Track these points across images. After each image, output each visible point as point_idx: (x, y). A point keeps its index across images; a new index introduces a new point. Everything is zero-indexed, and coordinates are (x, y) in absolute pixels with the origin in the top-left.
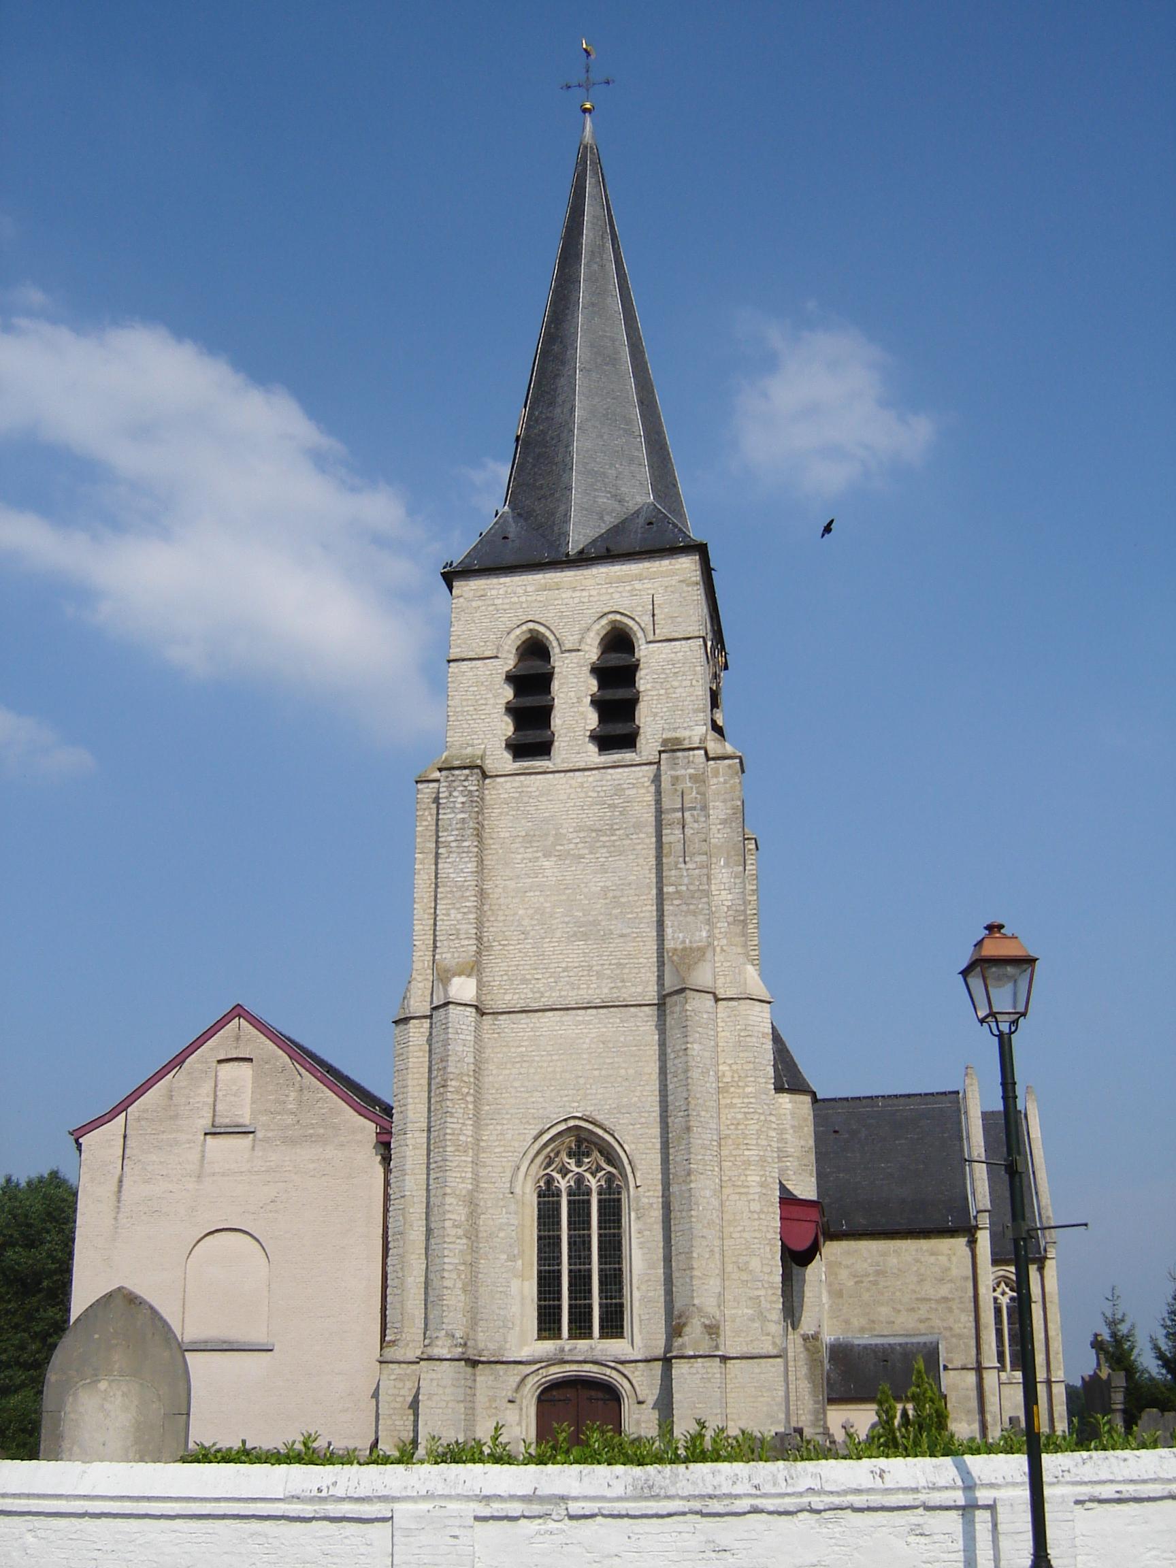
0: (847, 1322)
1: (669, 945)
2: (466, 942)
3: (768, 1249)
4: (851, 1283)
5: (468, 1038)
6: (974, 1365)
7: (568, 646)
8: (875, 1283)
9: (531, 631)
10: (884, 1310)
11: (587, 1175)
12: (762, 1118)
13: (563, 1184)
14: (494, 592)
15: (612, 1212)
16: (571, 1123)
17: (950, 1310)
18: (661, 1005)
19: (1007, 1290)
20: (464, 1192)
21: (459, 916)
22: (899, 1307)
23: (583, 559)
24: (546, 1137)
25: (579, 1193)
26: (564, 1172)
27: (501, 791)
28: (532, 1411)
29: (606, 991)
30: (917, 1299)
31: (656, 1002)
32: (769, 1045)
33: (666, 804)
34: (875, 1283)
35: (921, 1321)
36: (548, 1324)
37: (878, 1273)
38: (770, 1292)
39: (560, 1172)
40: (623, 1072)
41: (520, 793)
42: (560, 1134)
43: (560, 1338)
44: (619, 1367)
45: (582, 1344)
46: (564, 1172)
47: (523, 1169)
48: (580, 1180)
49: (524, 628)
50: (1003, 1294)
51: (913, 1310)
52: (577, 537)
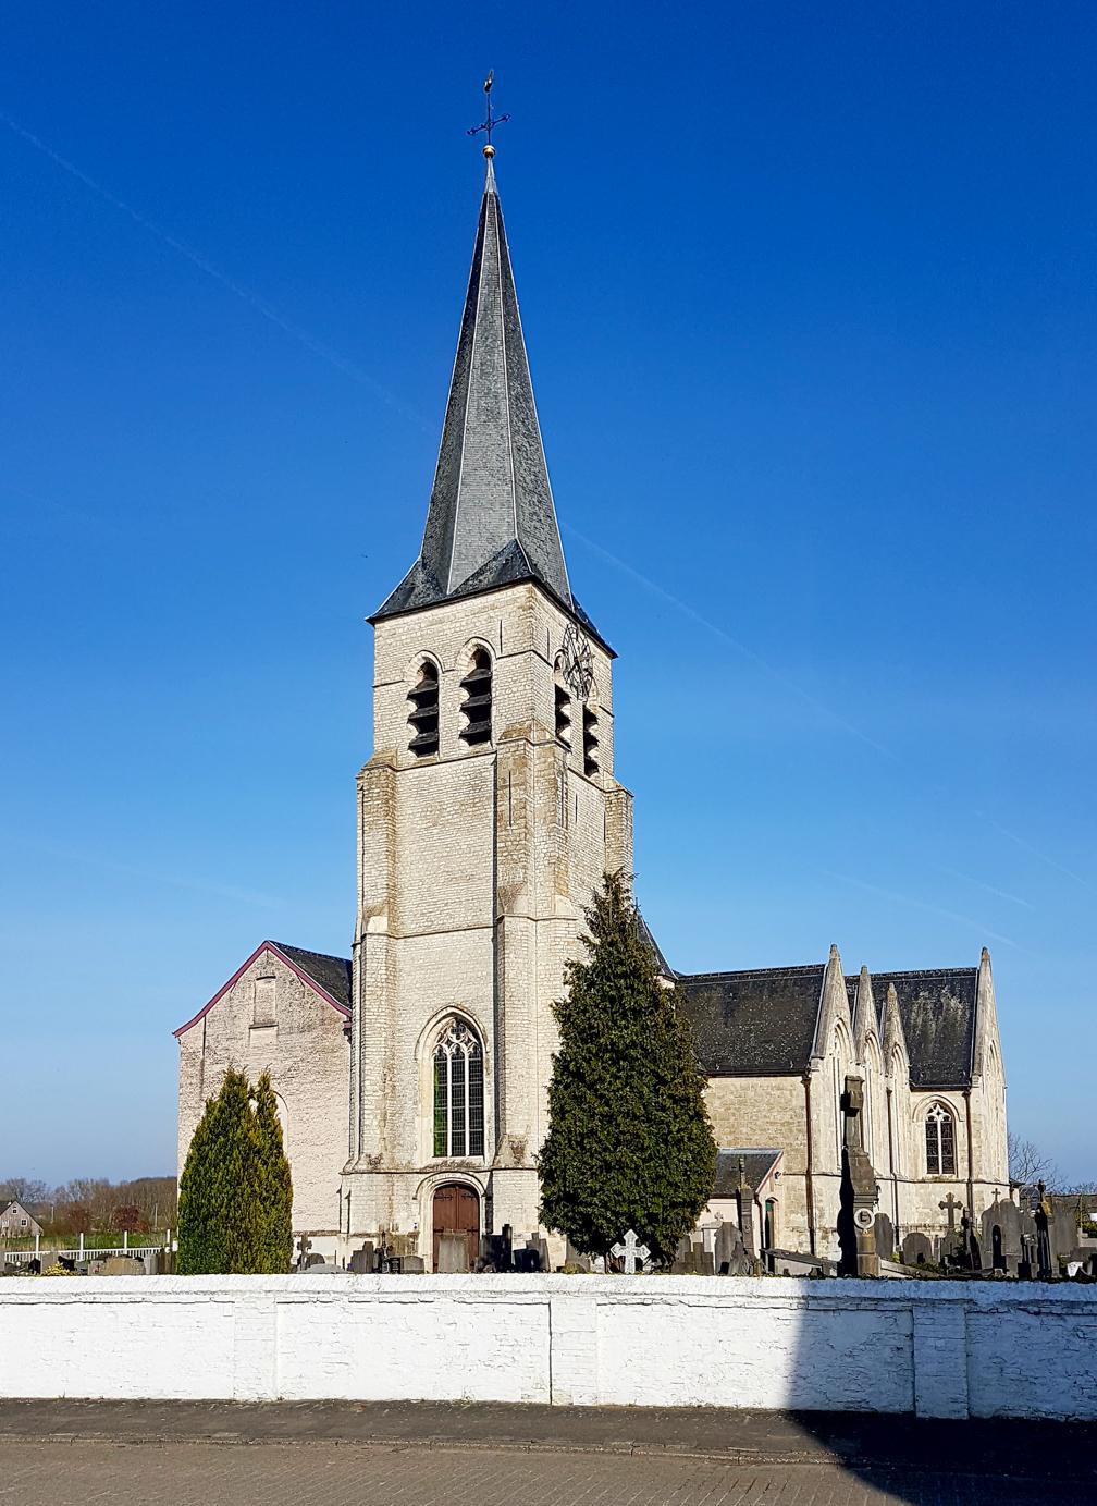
1: (499, 884)
2: (380, 891)
6: (813, 1177)
7: (448, 667)
8: (738, 1110)
9: (424, 658)
11: (462, 1045)
13: (448, 1051)
14: (401, 631)
15: (477, 1068)
16: (450, 1010)
17: (791, 1131)
18: (495, 927)
19: (941, 1111)
21: (377, 873)
23: (458, 597)
24: (440, 1016)
25: (458, 1054)
26: (449, 1043)
27: (406, 780)
28: (430, 1204)
29: (470, 918)
32: (582, 945)
33: (500, 783)
34: (738, 1110)
36: (440, 1150)
39: (447, 1043)
40: (479, 974)
41: (416, 779)
43: (464, 1155)
44: (476, 1175)
45: (458, 1159)
46: (449, 1043)
47: (422, 1042)
48: (458, 1049)
50: (938, 1114)
52: (453, 583)
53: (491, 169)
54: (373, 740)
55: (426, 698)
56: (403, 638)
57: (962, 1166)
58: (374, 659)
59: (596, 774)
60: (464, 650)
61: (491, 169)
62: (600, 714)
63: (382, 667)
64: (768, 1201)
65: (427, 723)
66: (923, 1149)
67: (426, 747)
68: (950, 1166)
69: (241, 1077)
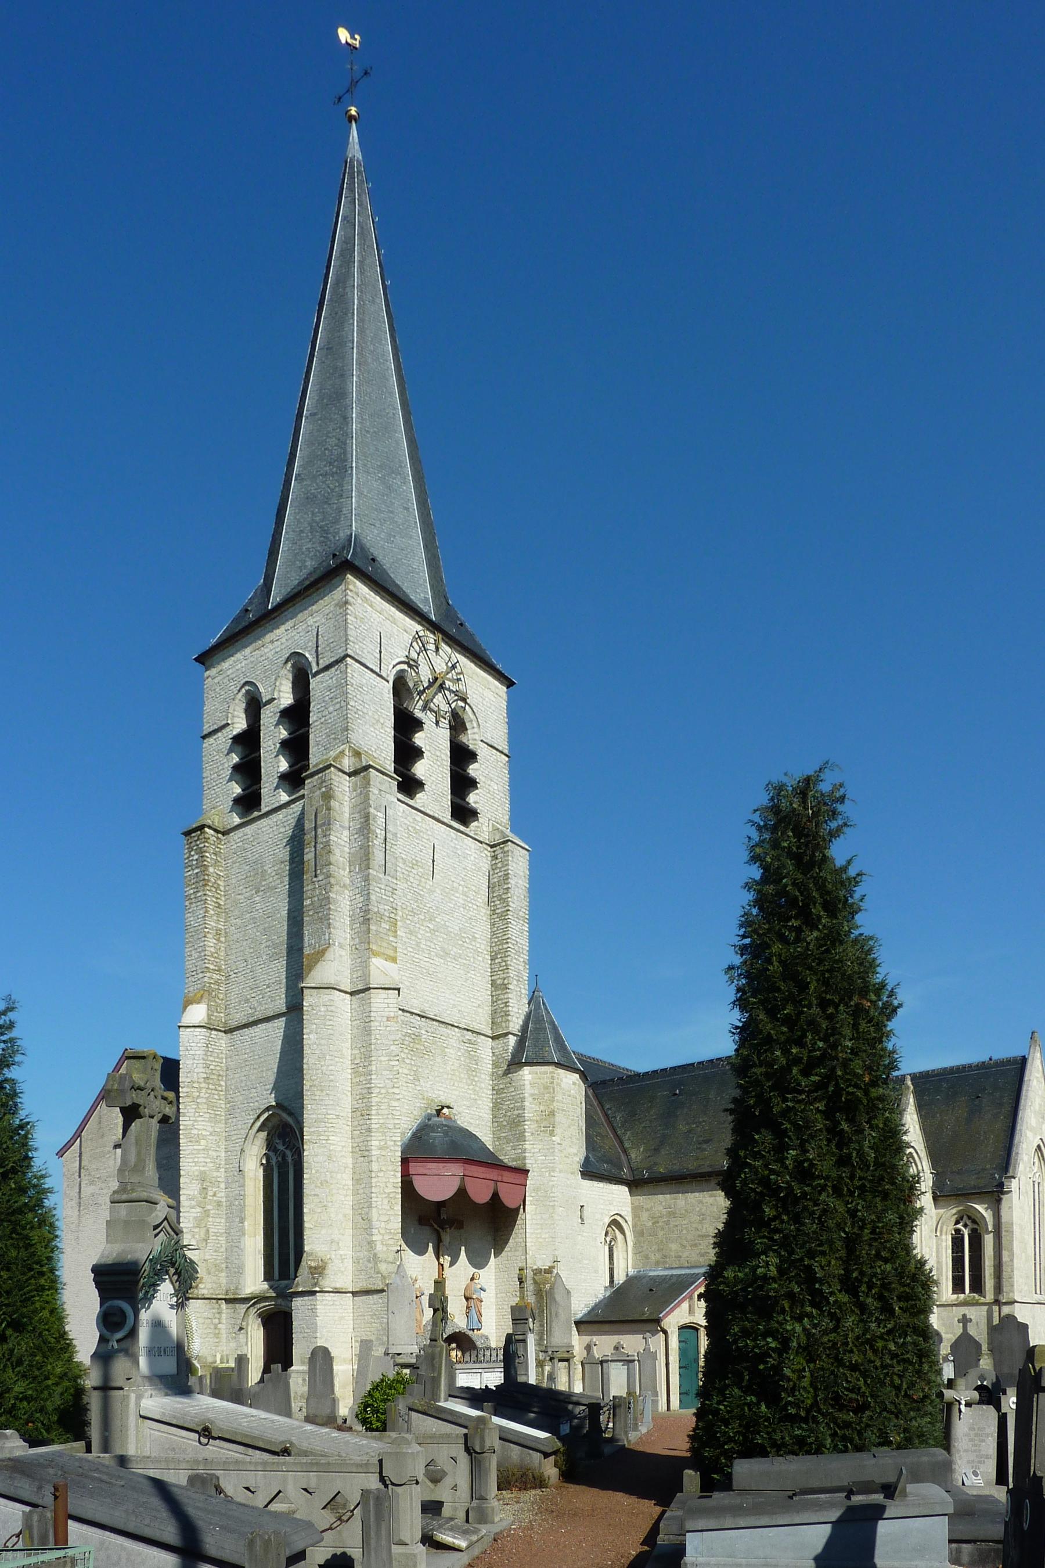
0: (647, 1257)
3: (386, 1201)
4: (650, 1224)
5: (198, 1052)
8: (667, 1223)
10: (674, 1246)
12: (383, 1091)
20: (196, 1173)
22: (685, 1243)
30: (699, 1236)
31: (284, 1010)
35: (702, 1255)
37: (670, 1214)
38: (387, 1237)
42: (267, 1119)
49: (243, 691)
51: (695, 1245)
53: (354, 132)
54: (202, 801)
55: (248, 742)
56: (229, 673)
57: (989, 1283)
58: (203, 704)
59: (475, 824)
60: (284, 672)
61: (354, 132)
62: (482, 751)
63: (211, 715)
64: (682, 1328)
65: (249, 770)
66: (236, 1213)
67: (249, 803)
68: (977, 1286)
69: (926, 1261)
